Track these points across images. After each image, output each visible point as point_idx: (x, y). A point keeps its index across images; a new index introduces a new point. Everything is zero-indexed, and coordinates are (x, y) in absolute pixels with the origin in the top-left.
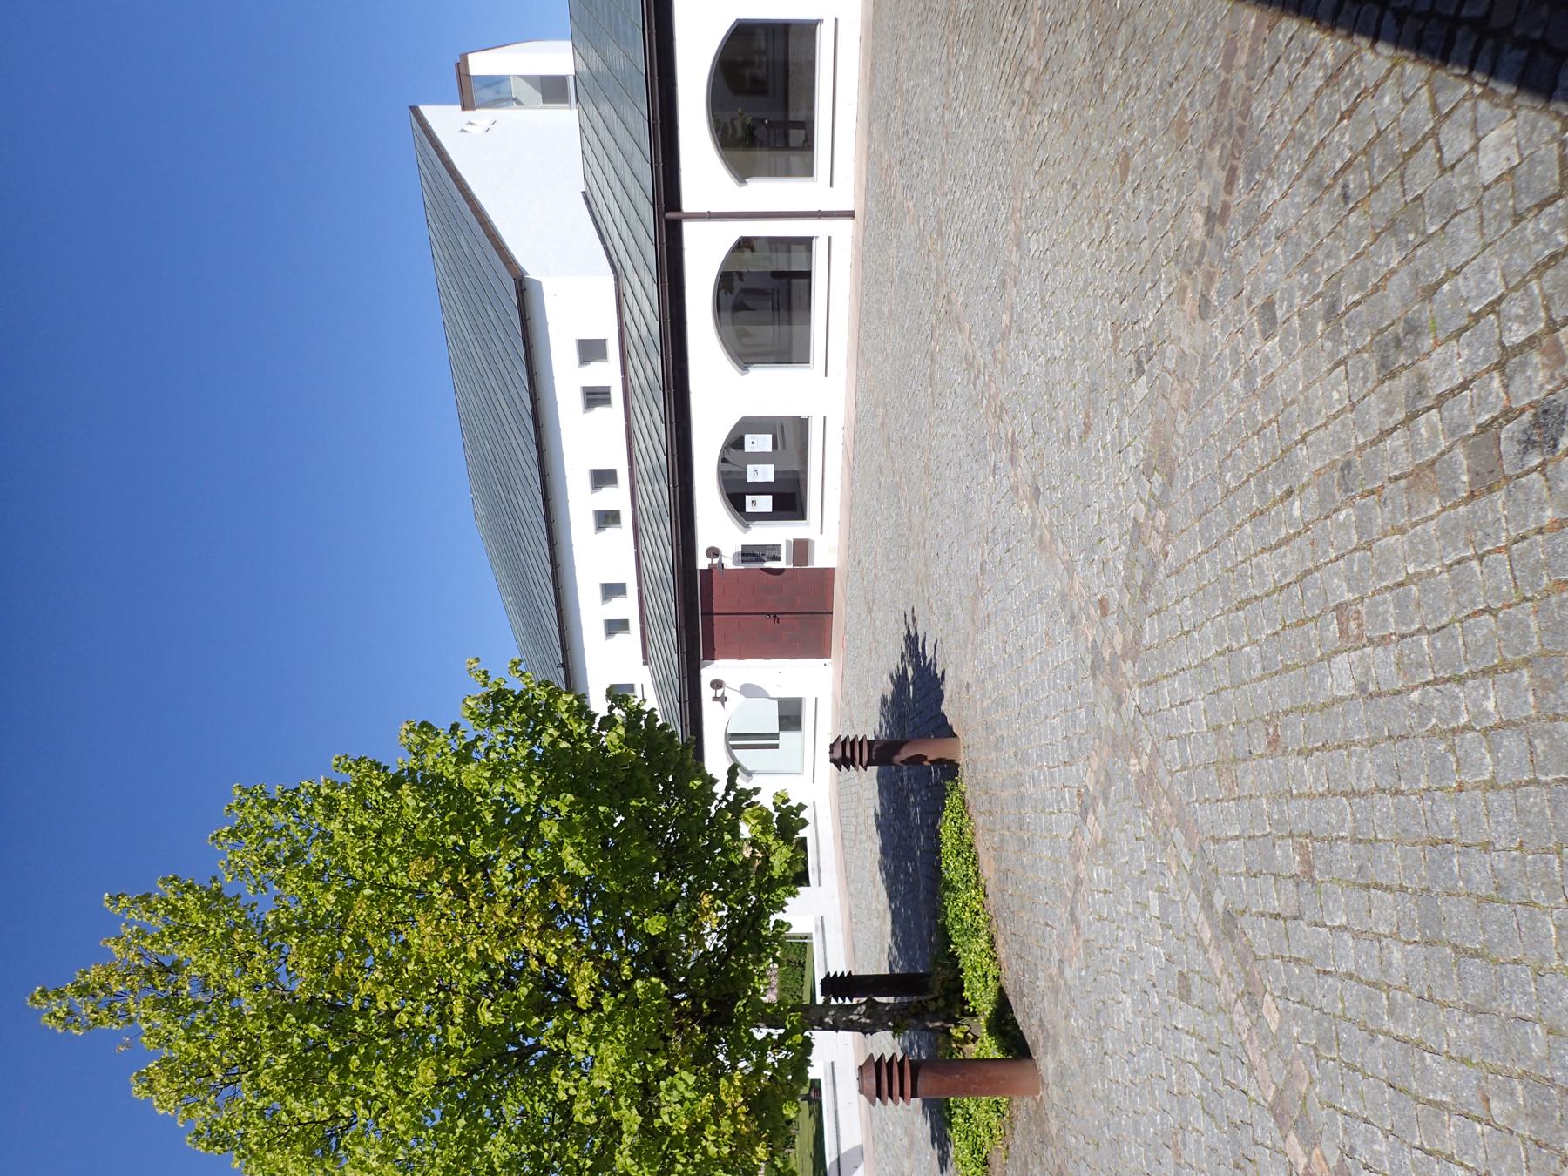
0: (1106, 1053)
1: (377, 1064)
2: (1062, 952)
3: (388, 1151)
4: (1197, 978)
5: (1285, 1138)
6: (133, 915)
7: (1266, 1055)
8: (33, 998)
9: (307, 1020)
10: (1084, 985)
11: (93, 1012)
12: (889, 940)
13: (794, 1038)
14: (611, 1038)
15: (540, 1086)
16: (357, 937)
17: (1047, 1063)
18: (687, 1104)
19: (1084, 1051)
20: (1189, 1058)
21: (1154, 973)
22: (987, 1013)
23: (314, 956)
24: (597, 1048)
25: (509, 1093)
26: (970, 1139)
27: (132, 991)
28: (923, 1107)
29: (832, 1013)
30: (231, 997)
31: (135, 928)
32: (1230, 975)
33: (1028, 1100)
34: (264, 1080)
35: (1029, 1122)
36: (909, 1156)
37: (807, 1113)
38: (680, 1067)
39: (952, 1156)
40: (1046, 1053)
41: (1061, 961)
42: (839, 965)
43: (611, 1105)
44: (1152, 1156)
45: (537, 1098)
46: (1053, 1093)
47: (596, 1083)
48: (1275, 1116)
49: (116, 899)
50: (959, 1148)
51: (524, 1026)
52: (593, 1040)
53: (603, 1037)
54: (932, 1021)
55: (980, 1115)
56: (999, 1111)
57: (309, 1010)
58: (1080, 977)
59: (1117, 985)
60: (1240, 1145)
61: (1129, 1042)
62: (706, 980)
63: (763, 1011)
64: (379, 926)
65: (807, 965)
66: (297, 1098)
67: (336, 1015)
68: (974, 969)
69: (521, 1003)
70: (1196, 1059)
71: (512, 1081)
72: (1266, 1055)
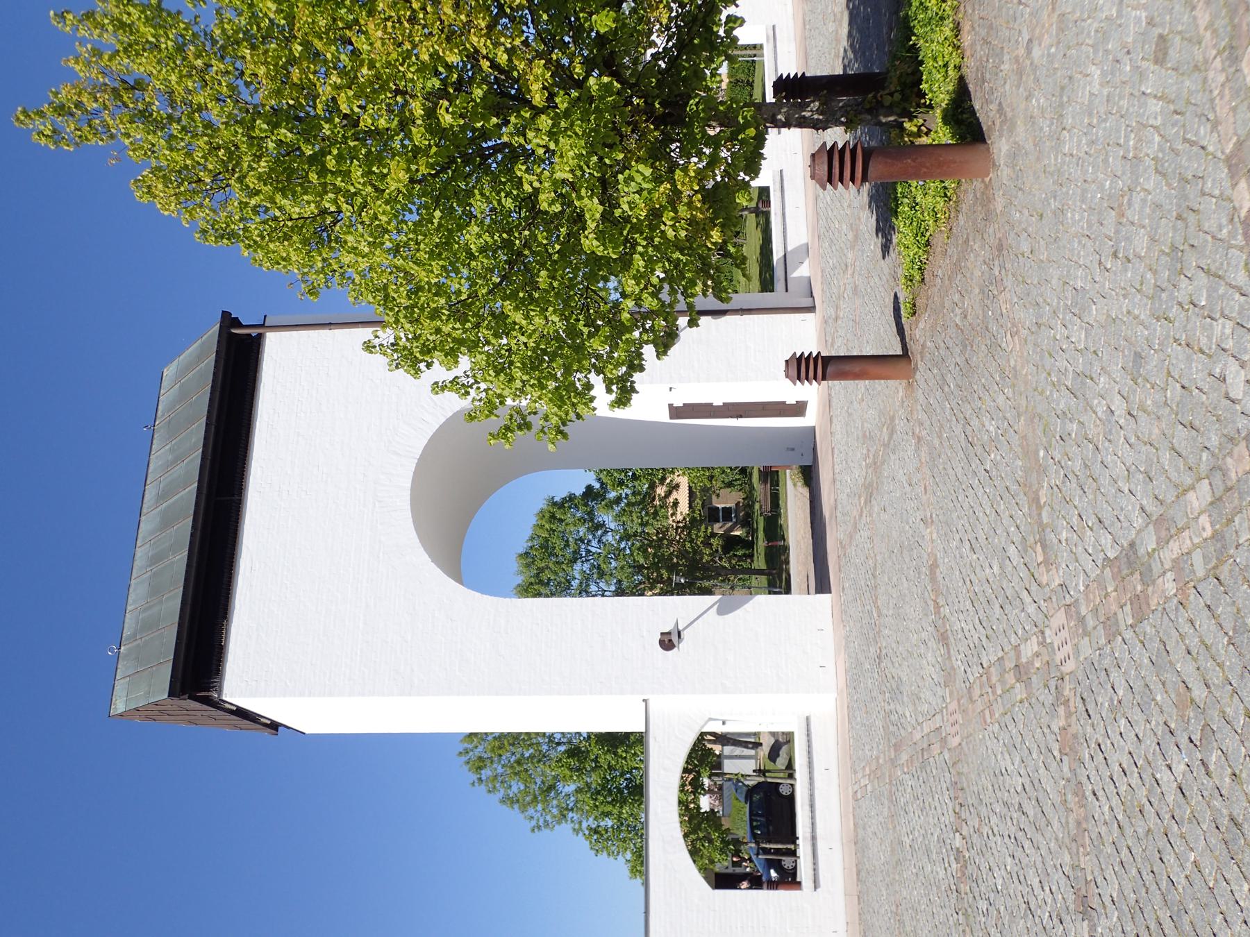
0: (1064, 129)
1: (352, 162)
2: (1033, 30)
3: (376, 238)
4: (1178, 39)
5: (1234, 186)
6: (82, 32)
7: (1234, 109)
8: (18, 119)
9: (276, 126)
10: (1052, 62)
11: (76, 129)
12: (845, 43)
13: (747, 132)
14: (569, 133)
15: (504, 184)
16: (306, 44)
17: (1000, 146)
18: (645, 193)
19: (1041, 129)
20: (1151, 122)
21: (1130, 40)
22: (943, 105)
23: (269, 63)
24: (557, 142)
25: (476, 191)
26: (915, 224)
27: (106, 108)
28: (870, 203)
29: (785, 110)
30: (200, 109)
31: (89, 46)
32: (1215, 31)
33: (977, 184)
34: (251, 181)
35: (974, 205)
36: (853, 248)
37: (754, 224)
38: (637, 162)
39: (895, 240)
40: (1001, 136)
41: (1030, 41)
42: (790, 66)
43: (574, 195)
44: (1094, 219)
45: (503, 194)
46: (1005, 173)
47: (559, 175)
48: (1230, 167)
49: (61, 16)
50: (903, 232)
51: (483, 125)
52: (552, 135)
53: (561, 132)
54: (886, 116)
55: (926, 202)
56: (946, 195)
57: (276, 118)
58: (1049, 55)
59: (1088, 57)
60: (1186, 198)
61: (1090, 115)
62: (658, 80)
63: (716, 109)
64: (327, 33)
65: (755, 85)
66: (285, 196)
67: (306, 125)
68: (935, 59)
69: (477, 105)
70: (1159, 122)
71: (478, 180)
72: (1234, 109)
